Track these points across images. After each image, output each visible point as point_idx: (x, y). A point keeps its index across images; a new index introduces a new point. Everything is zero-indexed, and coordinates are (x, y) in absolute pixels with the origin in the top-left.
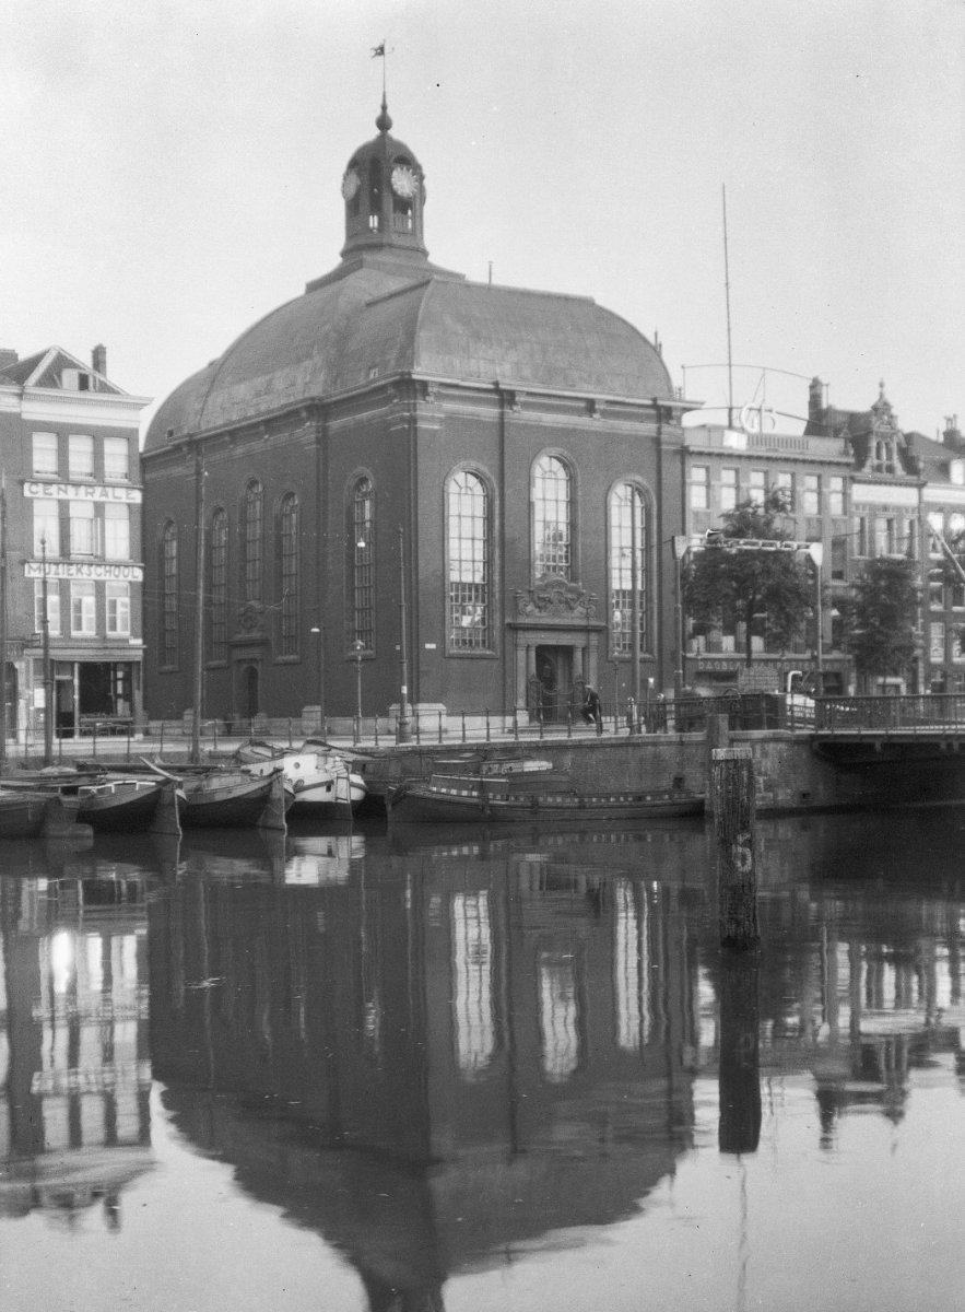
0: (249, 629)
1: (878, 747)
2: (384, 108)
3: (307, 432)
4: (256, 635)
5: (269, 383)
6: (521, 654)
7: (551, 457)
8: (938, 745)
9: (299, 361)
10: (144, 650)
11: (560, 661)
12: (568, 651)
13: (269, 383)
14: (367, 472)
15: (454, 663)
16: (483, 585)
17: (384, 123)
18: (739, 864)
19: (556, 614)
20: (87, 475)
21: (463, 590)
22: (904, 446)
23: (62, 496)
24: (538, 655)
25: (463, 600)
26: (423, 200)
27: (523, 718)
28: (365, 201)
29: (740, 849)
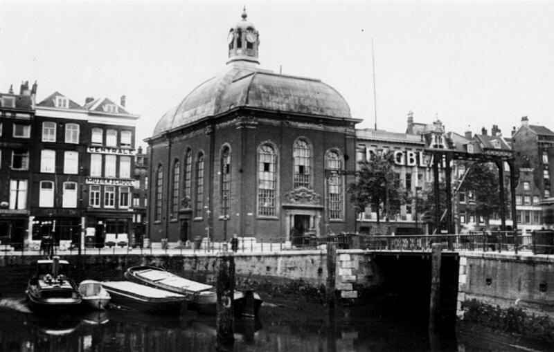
0: (186, 207)
1: (398, 257)
3: (208, 129)
4: (188, 209)
5: (196, 111)
6: (288, 218)
8: (396, 256)
9: (207, 102)
11: (305, 222)
12: (308, 217)
13: (196, 111)
14: (228, 145)
15: (260, 222)
18: (224, 304)
19: (302, 202)
21: (265, 192)
22: (447, 137)
23: (103, 152)
25: (265, 196)
26: (258, 44)
27: (288, 244)
28: (235, 44)
29: (225, 297)
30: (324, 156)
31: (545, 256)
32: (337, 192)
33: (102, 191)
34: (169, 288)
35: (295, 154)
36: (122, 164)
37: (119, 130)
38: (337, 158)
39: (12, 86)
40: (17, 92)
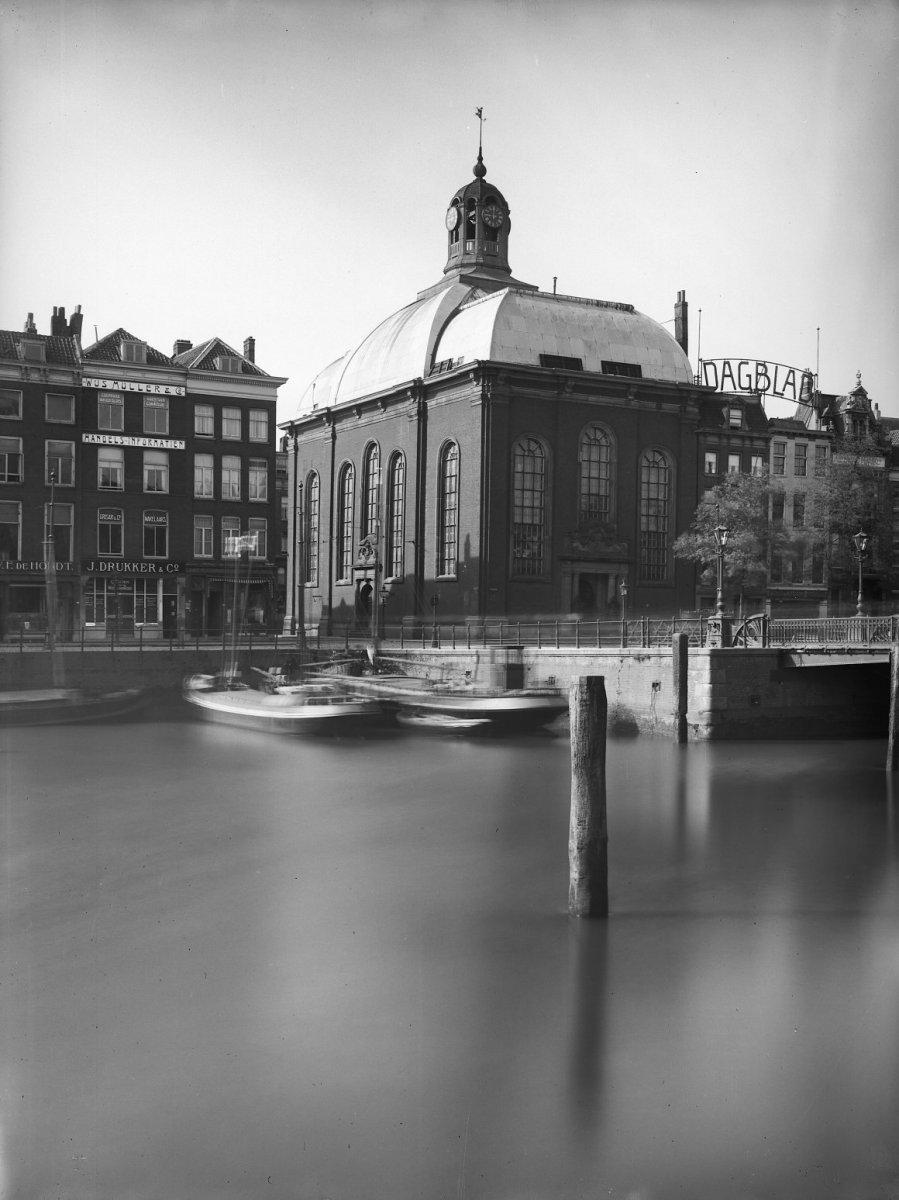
2: (480, 159)
6: (568, 580)
7: (595, 429)
10: (189, 691)
16: (540, 526)
17: (480, 170)
20: (310, 614)
24: (580, 581)
30: (638, 457)
31: (891, 737)
32: (537, 521)
33: (85, 519)
34: (236, 722)
35: (583, 456)
36: (252, 475)
37: (246, 406)
38: (662, 464)
39: (31, 316)
40: (44, 328)
